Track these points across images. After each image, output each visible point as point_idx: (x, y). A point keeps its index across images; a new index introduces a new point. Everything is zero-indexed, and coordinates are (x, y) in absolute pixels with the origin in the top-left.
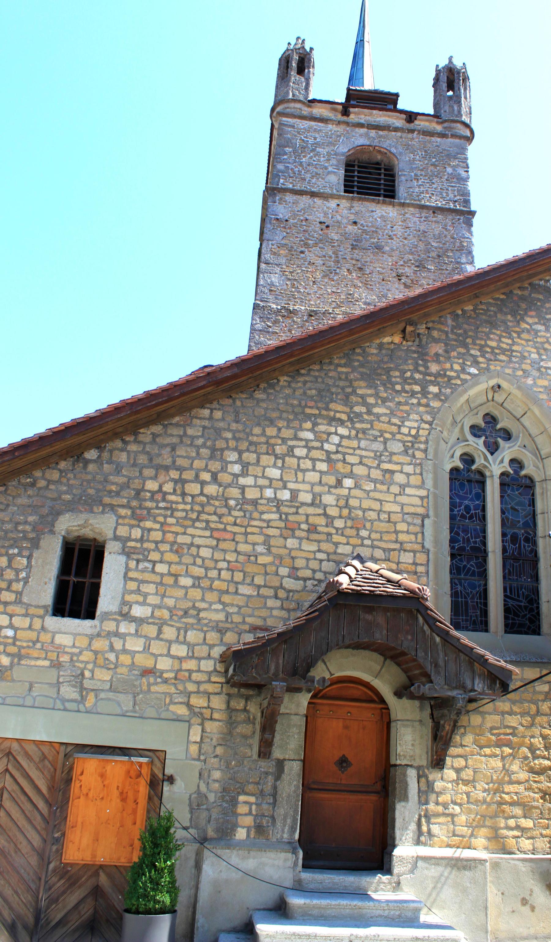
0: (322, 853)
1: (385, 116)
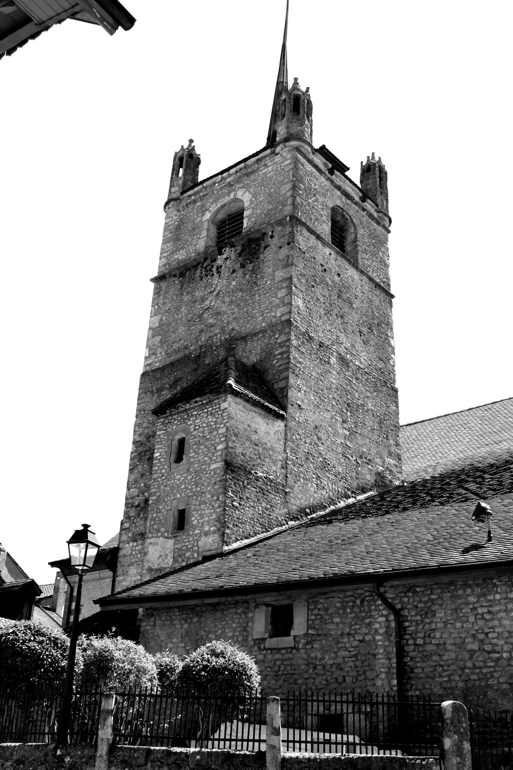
0: (337, 615)
1: (351, 188)
